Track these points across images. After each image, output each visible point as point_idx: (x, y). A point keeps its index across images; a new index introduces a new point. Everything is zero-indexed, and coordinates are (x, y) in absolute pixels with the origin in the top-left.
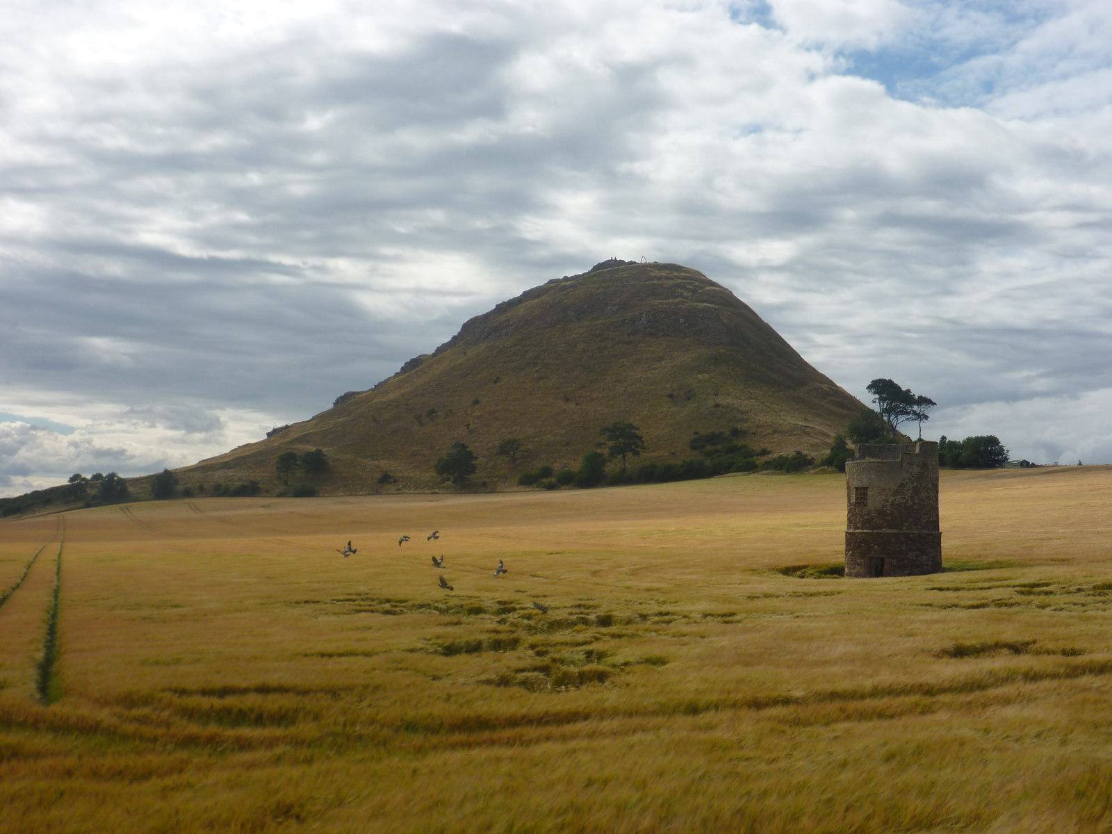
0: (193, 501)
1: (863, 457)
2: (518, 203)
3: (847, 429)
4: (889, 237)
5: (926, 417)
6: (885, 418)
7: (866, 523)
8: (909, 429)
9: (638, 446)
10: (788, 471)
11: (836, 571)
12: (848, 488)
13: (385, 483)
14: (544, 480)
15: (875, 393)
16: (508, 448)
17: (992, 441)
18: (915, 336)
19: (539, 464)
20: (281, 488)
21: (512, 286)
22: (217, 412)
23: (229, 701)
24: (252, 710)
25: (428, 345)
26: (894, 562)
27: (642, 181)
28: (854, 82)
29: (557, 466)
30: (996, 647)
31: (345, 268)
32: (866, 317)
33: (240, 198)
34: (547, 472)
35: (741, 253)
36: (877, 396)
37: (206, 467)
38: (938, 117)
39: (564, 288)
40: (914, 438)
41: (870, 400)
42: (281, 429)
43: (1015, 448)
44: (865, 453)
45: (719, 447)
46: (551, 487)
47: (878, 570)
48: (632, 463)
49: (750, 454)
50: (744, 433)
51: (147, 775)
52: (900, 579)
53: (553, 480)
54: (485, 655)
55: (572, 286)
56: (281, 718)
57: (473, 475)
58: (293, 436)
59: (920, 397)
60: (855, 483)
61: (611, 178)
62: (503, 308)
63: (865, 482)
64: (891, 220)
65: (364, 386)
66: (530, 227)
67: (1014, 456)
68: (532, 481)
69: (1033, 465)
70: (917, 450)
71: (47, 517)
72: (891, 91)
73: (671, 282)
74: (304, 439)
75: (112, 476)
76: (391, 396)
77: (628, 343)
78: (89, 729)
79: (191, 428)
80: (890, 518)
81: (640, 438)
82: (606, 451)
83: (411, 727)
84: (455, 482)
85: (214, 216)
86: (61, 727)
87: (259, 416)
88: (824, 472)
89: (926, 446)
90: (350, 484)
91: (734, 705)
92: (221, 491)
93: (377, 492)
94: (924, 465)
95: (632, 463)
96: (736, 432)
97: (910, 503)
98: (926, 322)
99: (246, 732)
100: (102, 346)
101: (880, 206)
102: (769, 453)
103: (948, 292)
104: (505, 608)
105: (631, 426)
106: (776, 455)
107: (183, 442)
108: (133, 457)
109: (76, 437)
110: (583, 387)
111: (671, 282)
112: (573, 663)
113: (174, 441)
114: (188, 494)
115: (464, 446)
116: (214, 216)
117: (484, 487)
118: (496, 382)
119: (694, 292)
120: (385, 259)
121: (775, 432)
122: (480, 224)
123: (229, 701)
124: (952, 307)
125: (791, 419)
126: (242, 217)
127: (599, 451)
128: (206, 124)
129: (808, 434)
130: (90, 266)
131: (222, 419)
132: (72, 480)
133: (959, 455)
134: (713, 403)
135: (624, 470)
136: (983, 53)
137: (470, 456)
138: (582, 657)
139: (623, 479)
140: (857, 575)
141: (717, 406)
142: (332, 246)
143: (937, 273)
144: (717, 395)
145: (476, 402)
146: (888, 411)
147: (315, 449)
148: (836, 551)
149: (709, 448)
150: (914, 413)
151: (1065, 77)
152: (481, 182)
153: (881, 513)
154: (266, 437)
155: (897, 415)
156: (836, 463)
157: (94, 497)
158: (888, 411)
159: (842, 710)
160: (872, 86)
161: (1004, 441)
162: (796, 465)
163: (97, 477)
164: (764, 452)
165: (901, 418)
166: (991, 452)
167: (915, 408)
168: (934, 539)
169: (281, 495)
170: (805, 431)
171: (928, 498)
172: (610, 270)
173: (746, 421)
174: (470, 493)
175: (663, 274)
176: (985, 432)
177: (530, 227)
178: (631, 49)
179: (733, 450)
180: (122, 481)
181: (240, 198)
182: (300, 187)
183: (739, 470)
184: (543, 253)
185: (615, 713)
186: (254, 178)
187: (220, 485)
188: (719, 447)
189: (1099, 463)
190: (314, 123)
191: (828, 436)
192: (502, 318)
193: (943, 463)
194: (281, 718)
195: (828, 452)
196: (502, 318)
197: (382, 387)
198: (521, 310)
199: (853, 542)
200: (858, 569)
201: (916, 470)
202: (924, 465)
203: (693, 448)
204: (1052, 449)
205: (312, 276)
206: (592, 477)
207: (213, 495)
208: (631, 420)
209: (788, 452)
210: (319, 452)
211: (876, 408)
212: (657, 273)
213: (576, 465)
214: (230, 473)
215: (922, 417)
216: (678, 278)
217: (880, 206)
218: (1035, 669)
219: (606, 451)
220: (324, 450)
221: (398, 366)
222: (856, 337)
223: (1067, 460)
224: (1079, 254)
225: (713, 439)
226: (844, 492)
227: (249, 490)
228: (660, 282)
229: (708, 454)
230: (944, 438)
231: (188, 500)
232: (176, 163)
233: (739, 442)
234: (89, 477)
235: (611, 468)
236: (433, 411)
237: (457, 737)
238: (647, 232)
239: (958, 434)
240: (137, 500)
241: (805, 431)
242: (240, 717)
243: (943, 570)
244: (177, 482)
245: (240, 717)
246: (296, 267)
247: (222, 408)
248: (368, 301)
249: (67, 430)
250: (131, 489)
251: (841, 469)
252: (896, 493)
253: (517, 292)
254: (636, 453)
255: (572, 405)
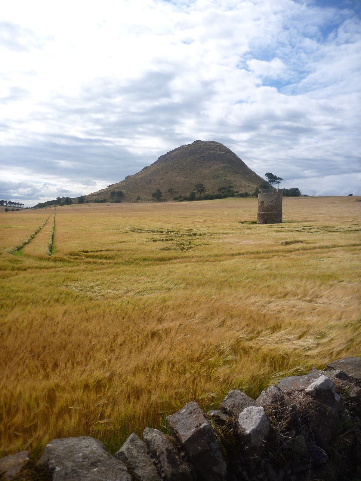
0: (89, 204)
1: (263, 193)
2: (172, 122)
3: (259, 186)
4: (275, 133)
5: (280, 183)
6: (269, 183)
7: (263, 210)
8: (276, 186)
9: (204, 190)
10: (243, 197)
11: (255, 223)
12: (259, 201)
13: (138, 199)
14: (180, 199)
15: (267, 176)
16: (170, 191)
17: (297, 189)
18: (280, 161)
19: (179, 195)
20: (112, 201)
21: (172, 146)
22: (95, 181)
23: (99, 253)
24: (104, 255)
25: (150, 162)
26: (270, 220)
27: (207, 116)
28: (269, 88)
29: (183, 195)
30: (298, 242)
31: (124, 141)
32: (269, 156)
33: (97, 122)
34: (180, 197)
35: (233, 137)
36: (267, 177)
37: (92, 195)
38: (291, 98)
39: (185, 148)
40: (277, 188)
41: (265, 178)
42: (111, 185)
43: (303, 191)
44: (264, 192)
45: (225, 191)
46: (181, 201)
47: (265, 223)
48: (203, 195)
49: (233, 192)
50: (232, 187)
51: (50, 268)
52: (275, 224)
53: (182, 199)
54: (164, 242)
55: (187, 147)
56: (110, 258)
57: (161, 198)
58: (115, 187)
59: (279, 178)
60: (261, 200)
61: (199, 115)
62: (169, 153)
63: (263, 200)
64: (277, 127)
65: (132, 174)
66: (178, 129)
67: (303, 193)
68: (176, 199)
69: (308, 196)
70: (277, 191)
71: (52, 208)
72: (279, 91)
73: (213, 146)
74: (117, 188)
75: (67, 197)
76: (140, 177)
77: (202, 163)
78: (61, 260)
79: (88, 184)
80: (269, 209)
81: (205, 188)
82: (196, 191)
83: (145, 259)
84: (156, 199)
85: (90, 127)
86: (55, 260)
87: (105, 182)
88: (252, 197)
89: (280, 190)
90: (130, 200)
91: (227, 255)
92: (96, 201)
93: (137, 202)
94: (279, 195)
95: (203, 195)
96: (230, 187)
97: (275, 205)
98: (284, 157)
99: (103, 261)
100: (63, 163)
101: (273, 123)
102: (238, 192)
103: (291, 149)
104: (169, 231)
105: (202, 185)
106: (240, 193)
107: (86, 188)
108: (71, 192)
109: (58, 187)
110: (190, 174)
111: (213, 146)
112: (186, 245)
113: (83, 188)
114: (87, 202)
115: (159, 190)
116: (90, 127)
117: (164, 201)
118: (167, 173)
119: (220, 149)
120: (137, 139)
121: (240, 187)
122: (163, 129)
123: (99, 253)
124: (292, 153)
125: (244, 183)
126: (99, 127)
127: (194, 191)
128: (89, 99)
129: (249, 187)
130: (57, 141)
131: (96, 183)
132: (57, 198)
133: (288, 193)
134: (224, 179)
135: (200, 196)
136: (292, 83)
137: (161, 193)
138: (188, 243)
139: (200, 199)
140: (260, 224)
141: (225, 180)
142: (121, 135)
143: (288, 142)
144: (225, 177)
145: (162, 178)
146: (270, 181)
147: (120, 190)
148: (255, 218)
149: (223, 191)
150: (277, 182)
151: (314, 90)
152: (163, 116)
153: (267, 208)
154: (107, 187)
155: (272, 182)
156: (256, 195)
157: (63, 203)
158: (270, 181)
159: (255, 256)
160: (274, 89)
161: (301, 189)
162: (245, 195)
163: (64, 198)
164: (237, 192)
165: (273, 183)
166: (297, 192)
167: (277, 181)
168: (280, 215)
169: (112, 202)
170: (248, 186)
171: (280, 204)
172: (197, 142)
173: (232, 184)
174: (162, 202)
175: (212, 144)
176: (295, 187)
177: (178, 129)
178: (207, 76)
179: (229, 191)
180: (70, 199)
181: (97, 122)
182: (113, 118)
183: (230, 196)
184: (179, 137)
185: (196, 257)
186: (100, 116)
187: (96, 200)
188: (225, 191)
189: (326, 196)
190: (118, 100)
191: (254, 187)
192: (169, 156)
193: (284, 195)
194: (110, 258)
195: (254, 192)
196: (169, 156)
197: (137, 174)
198: (174, 154)
199: (260, 215)
200: (260, 222)
201: (277, 196)
202: (279, 195)
203: (219, 191)
204: (314, 192)
205: (118, 144)
206: (192, 198)
207: (94, 202)
208: (202, 183)
209: (244, 192)
210: (121, 191)
211: (267, 180)
212: (210, 144)
213: (188, 195)
214: (98, 197)
215: (279, 183)
216: (215, 145)
217: (273, 123)
218: (305, 247)
219: (196, 191)
220: (123, 191)
221: (142, 168)
222: (265, 161)
223: (317, 194)
224: (329, 138)
225: (224, 188)
226: (258, 202)
227: (103, 201)
228: (211, 146)
229: (222, 193)
230: (284, 188)
231: (87, 204)
232: (80, 111)
233: (231, 189)
234: (61, 197)
235: (197, 196)
236: (151, 181)
237: (156, 262)
238: (208, 131)
239: (288, 188)
240: (74, 204)
241: (248, 186)
242: (101, 257)
243: (283, 223)
244: (84, 199)
245: (101, 257)
246: (112, 141)
247: (97, 180)
248: (130, 150)
249: (55, 185)
250: (72, 201)
251: (257, 196)
252: (271, 202)
253: (173, 149)
254: (204, 192)
255: (187, 179)
